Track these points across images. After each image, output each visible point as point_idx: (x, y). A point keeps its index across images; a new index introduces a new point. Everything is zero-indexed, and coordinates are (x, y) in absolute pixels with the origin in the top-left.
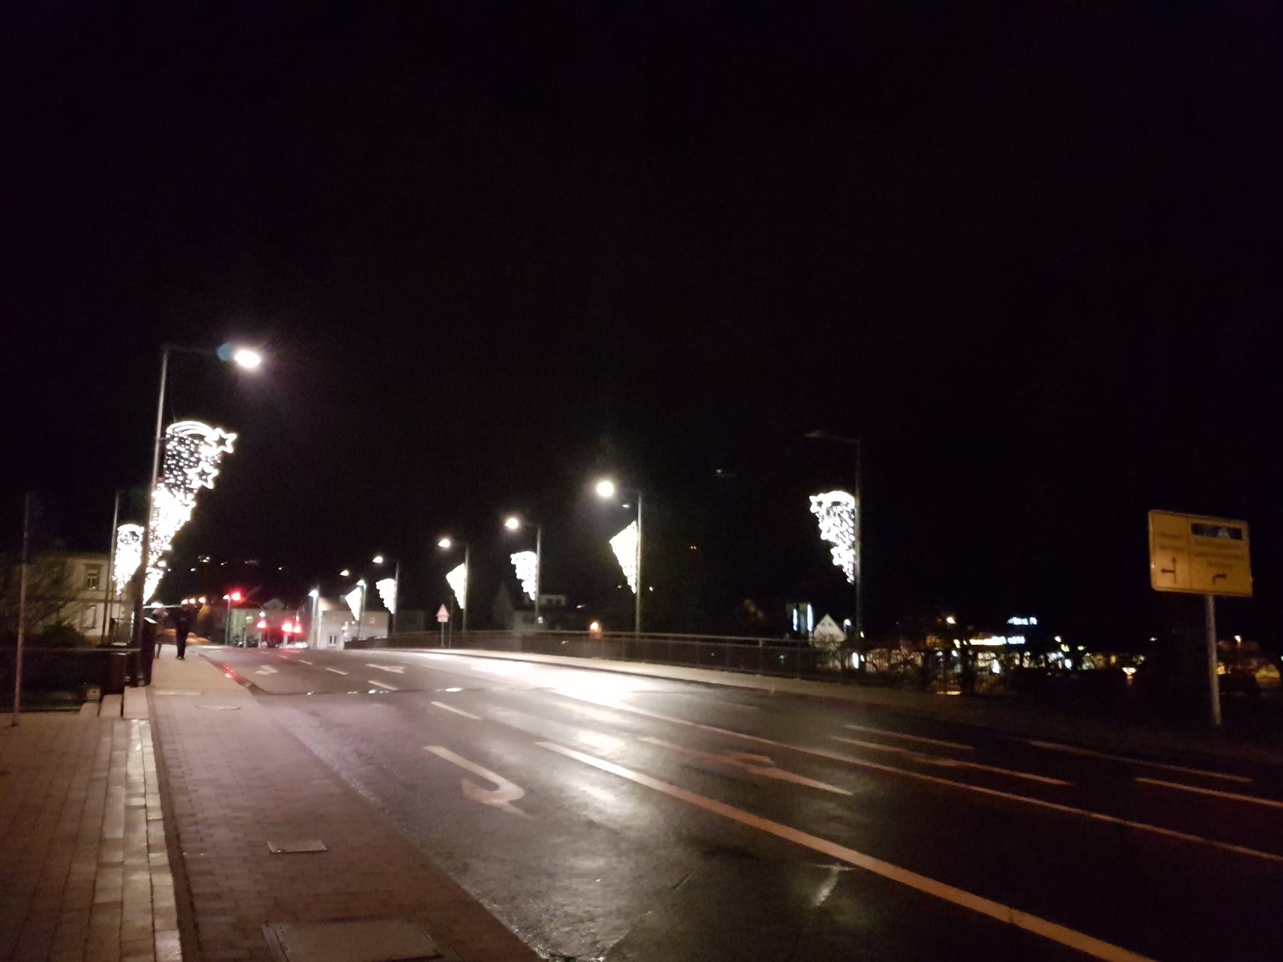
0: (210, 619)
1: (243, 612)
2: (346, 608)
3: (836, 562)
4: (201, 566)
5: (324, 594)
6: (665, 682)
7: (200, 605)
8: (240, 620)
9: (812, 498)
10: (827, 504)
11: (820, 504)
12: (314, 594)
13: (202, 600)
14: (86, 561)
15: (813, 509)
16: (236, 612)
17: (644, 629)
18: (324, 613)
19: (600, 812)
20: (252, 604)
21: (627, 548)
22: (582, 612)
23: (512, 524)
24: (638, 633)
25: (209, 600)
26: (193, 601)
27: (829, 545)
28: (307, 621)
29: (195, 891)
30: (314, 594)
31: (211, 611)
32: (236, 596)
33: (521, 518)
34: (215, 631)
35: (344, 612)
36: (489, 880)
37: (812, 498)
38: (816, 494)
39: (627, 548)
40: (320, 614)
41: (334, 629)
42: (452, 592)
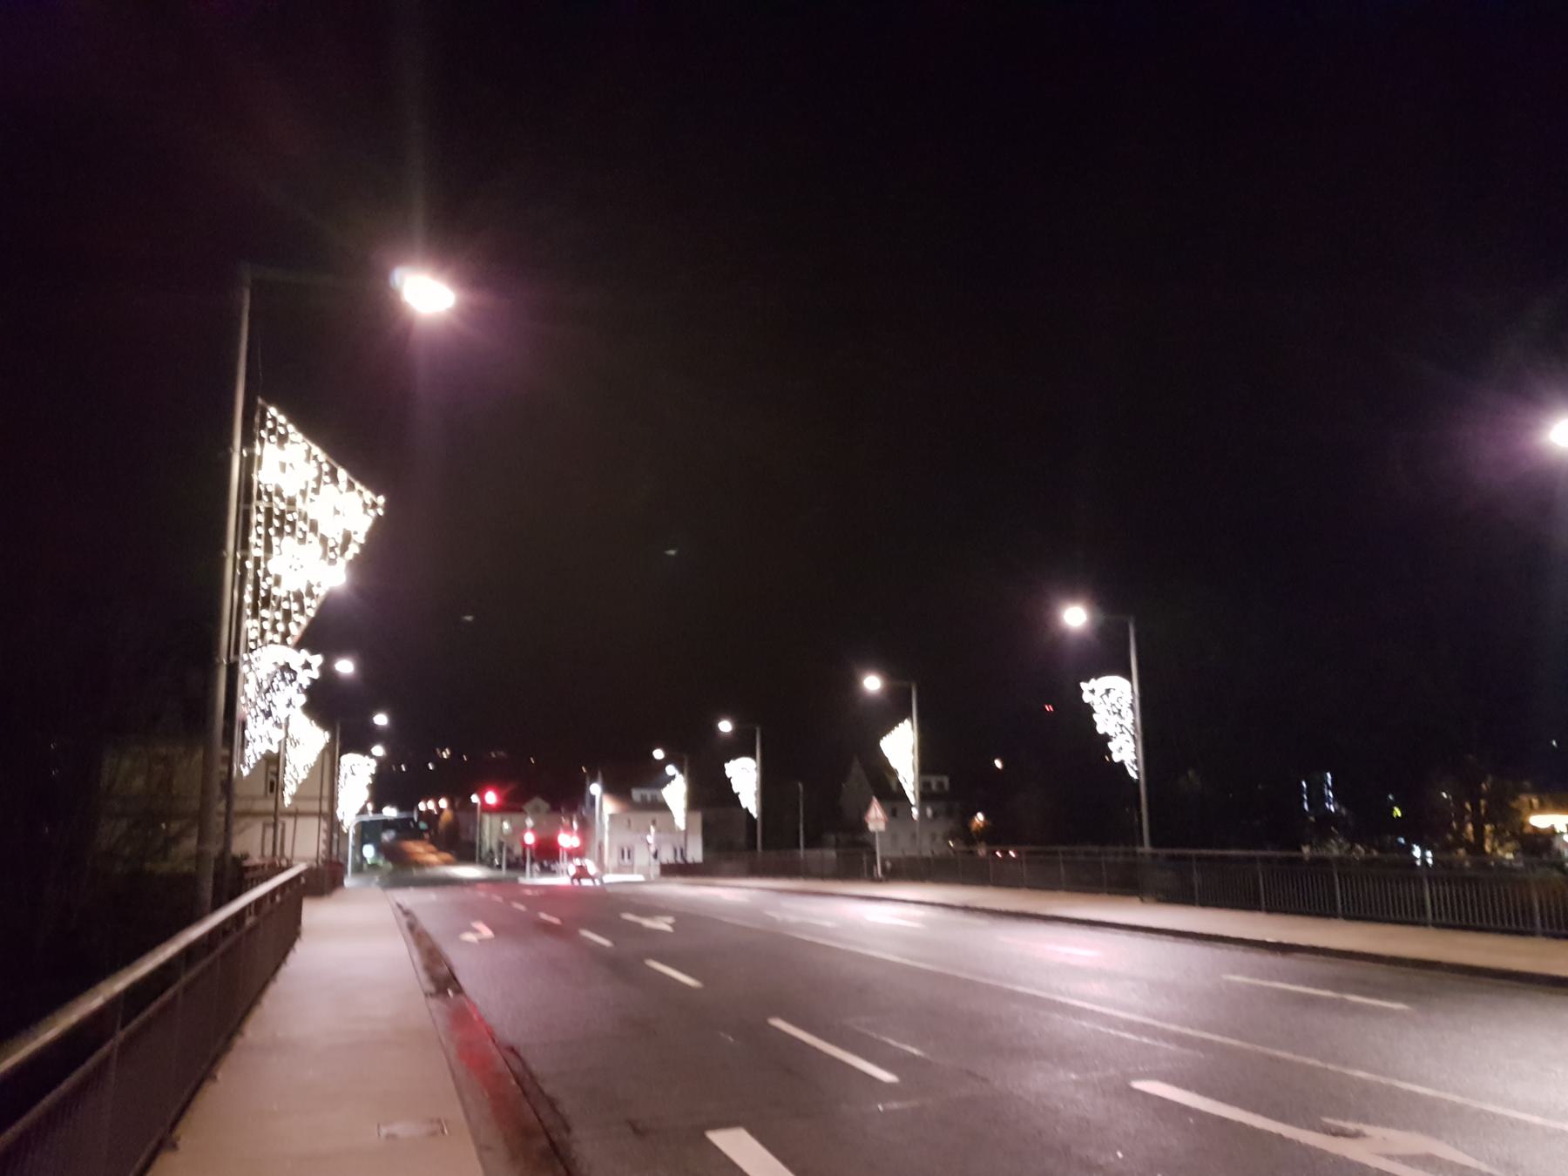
0: (454, 827)
1: (496, 819)
2: (663, 807)
3: (1116, 758)
4: (439, 762)
5: (609, 789)
7: (441, 811)
8: (494, 829)
9: (1083, 685)
10: (1100, 691)
11: (1093, 691)
12: (595, 789)
13: (443, 803)
14: (360, 538)
15: (1087, 697)
16: (487, 818)
17: (1153, 844)
18: (611, 816)
19: (242, 831)
20: (511, 805)
21: (1113, 705)
23: (872, 683)
24: (1147, 848)
25: (451, 805)
26: (431, 805)
27: (1106, 738)
28: (586, 828)
30: (595, 789)
31: (455, 818)
32: (491, 798)
33: (1092, 621)
34: (461, 845)
35: (657, 816)
37: (1083, 685)
38: (1087, 680)
39: (1113, 705)
40: (606, 819)
41: (627, 838)
42: (894, 773)
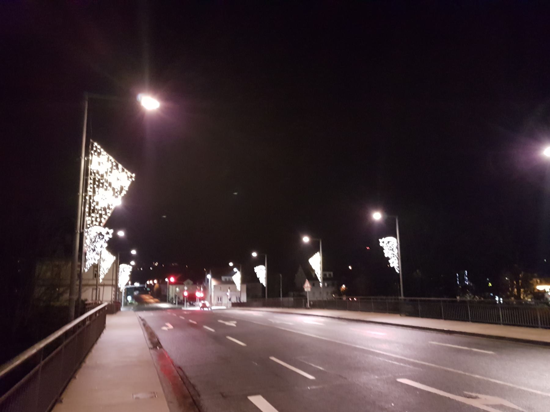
0: (159, 290)
1: (174, 287)
2: (232, 283)
3: (392, 266)
4: (154, 267)
5: (214, 276)
6: (330, 319)
7: (155, 284)
8: (173, 291)
9: (380, 240)
10: (386, 242)
11: (383, 242)
12: (209, 276)
13: (155, 281)
14: (126, 189)
15: (381, 244)
16: (171, 287)
17: (405, 296)
18: (214, 286)
19: (85, 291)
20: (179, 282)
21: (390, 247)
23: (306, 239)
24: (402, 297)
25: (158, 282)
26: (151, 282)
27: (388, 259)
28: (206, 290)
29: (105, 288)
30: (209, 276)
31: (160, 286)
32: (172, 279)
33: (383, 217)
34: (162, 296)
35: (231, 286)
36: (155, 344)
37: (380, 240)
38: (381, 238)
39: (390, 247)
40: (213, 287)
41: (220, 294)
42: (314, 271)
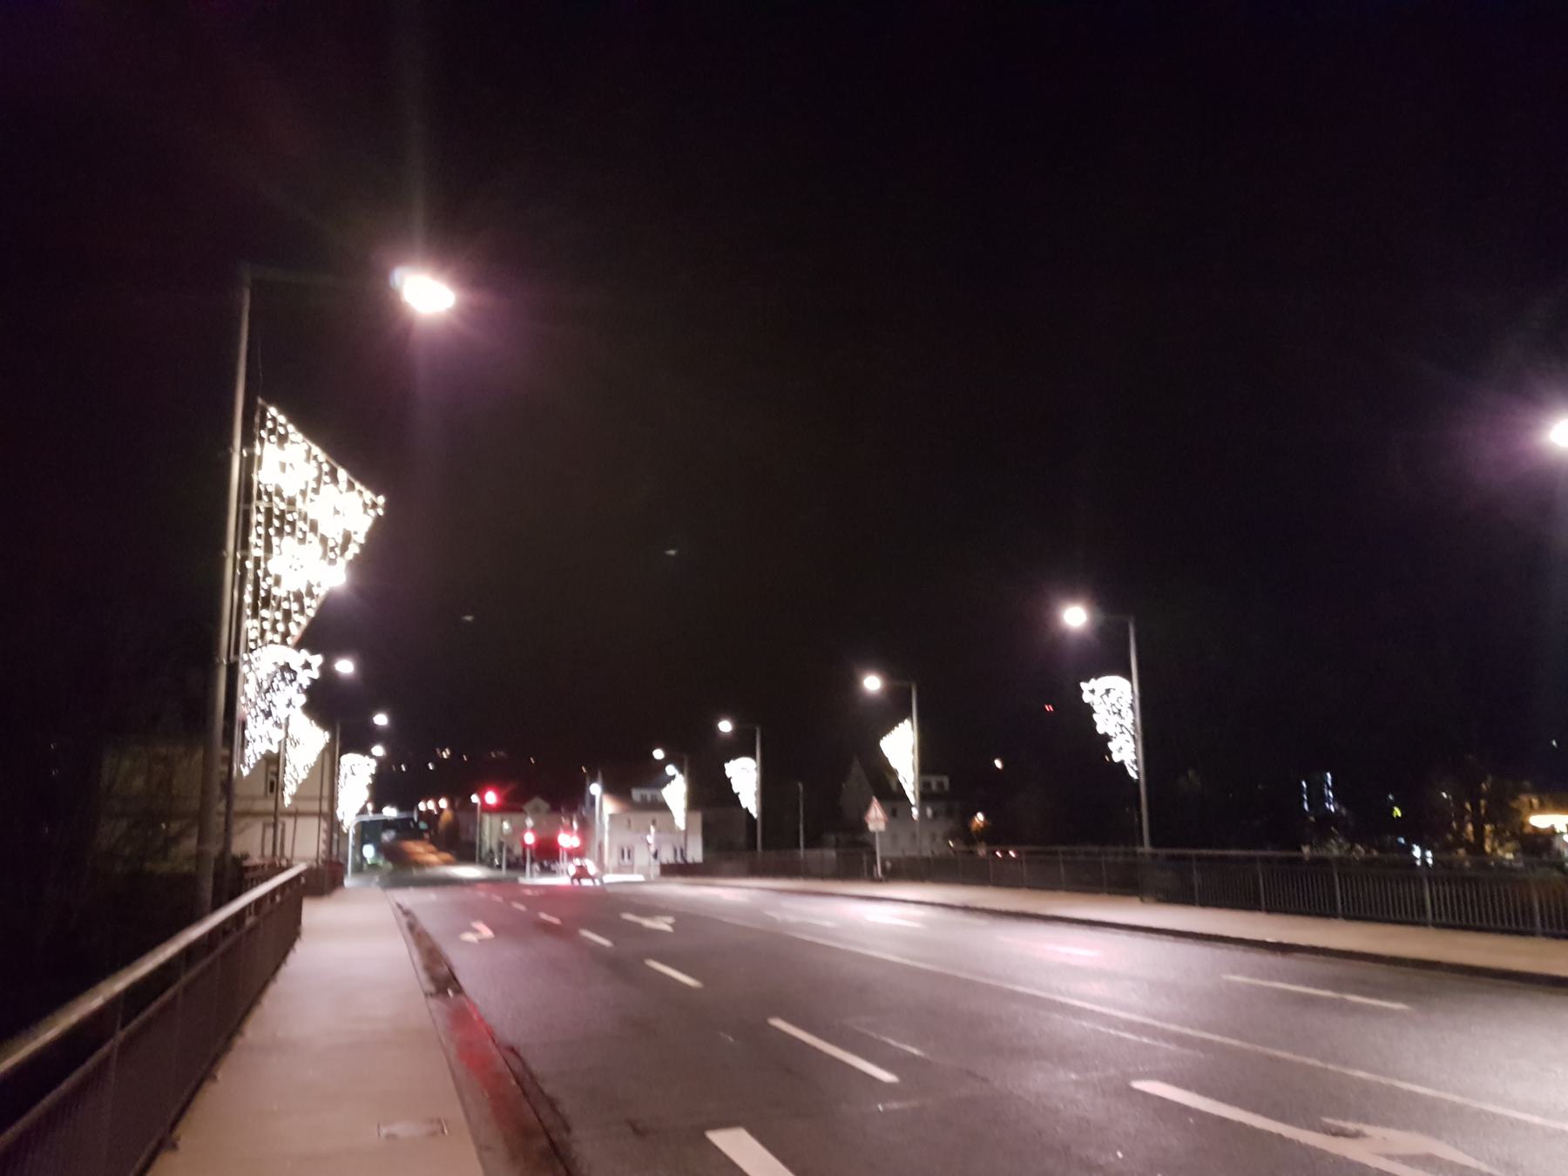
0: (454, 827)
1: (496, 819)
2: (663, 807)
3: (1116, 758)
4: (439, 762)
5: (609, 789)
6: (941, 910)
7: (441, 811)
8: (494, 829)
9: (1083, 685)
10: (1100, 691)
11: (1093, 691)
12: (595, 789)
13: (443, 803)
14: (360, 538)
15: (1087, 697)
16: (487, 818)
17: (1153, 844)
18: (611, 816)
19: (242, 831)
20: (511, 805)
21: (1113, 705)
22: (1036, 818)
23: (872, 683)
24: (1147, 848)
25: (451, 805)
26: (431, 805)
27: (1106, 738)
28: (586, 828)
29: (301, 821)
30: (595, 789)
31: (455, 818)
32: (491, 798)
33: (1092, 621)
34: (461, 845)
35: (657, 816)
37: (1083, 685)
38: (1087, 680)
39: (1113, 705)
40: (606, 819)
41: (627, 838)
42: (894, 773)
